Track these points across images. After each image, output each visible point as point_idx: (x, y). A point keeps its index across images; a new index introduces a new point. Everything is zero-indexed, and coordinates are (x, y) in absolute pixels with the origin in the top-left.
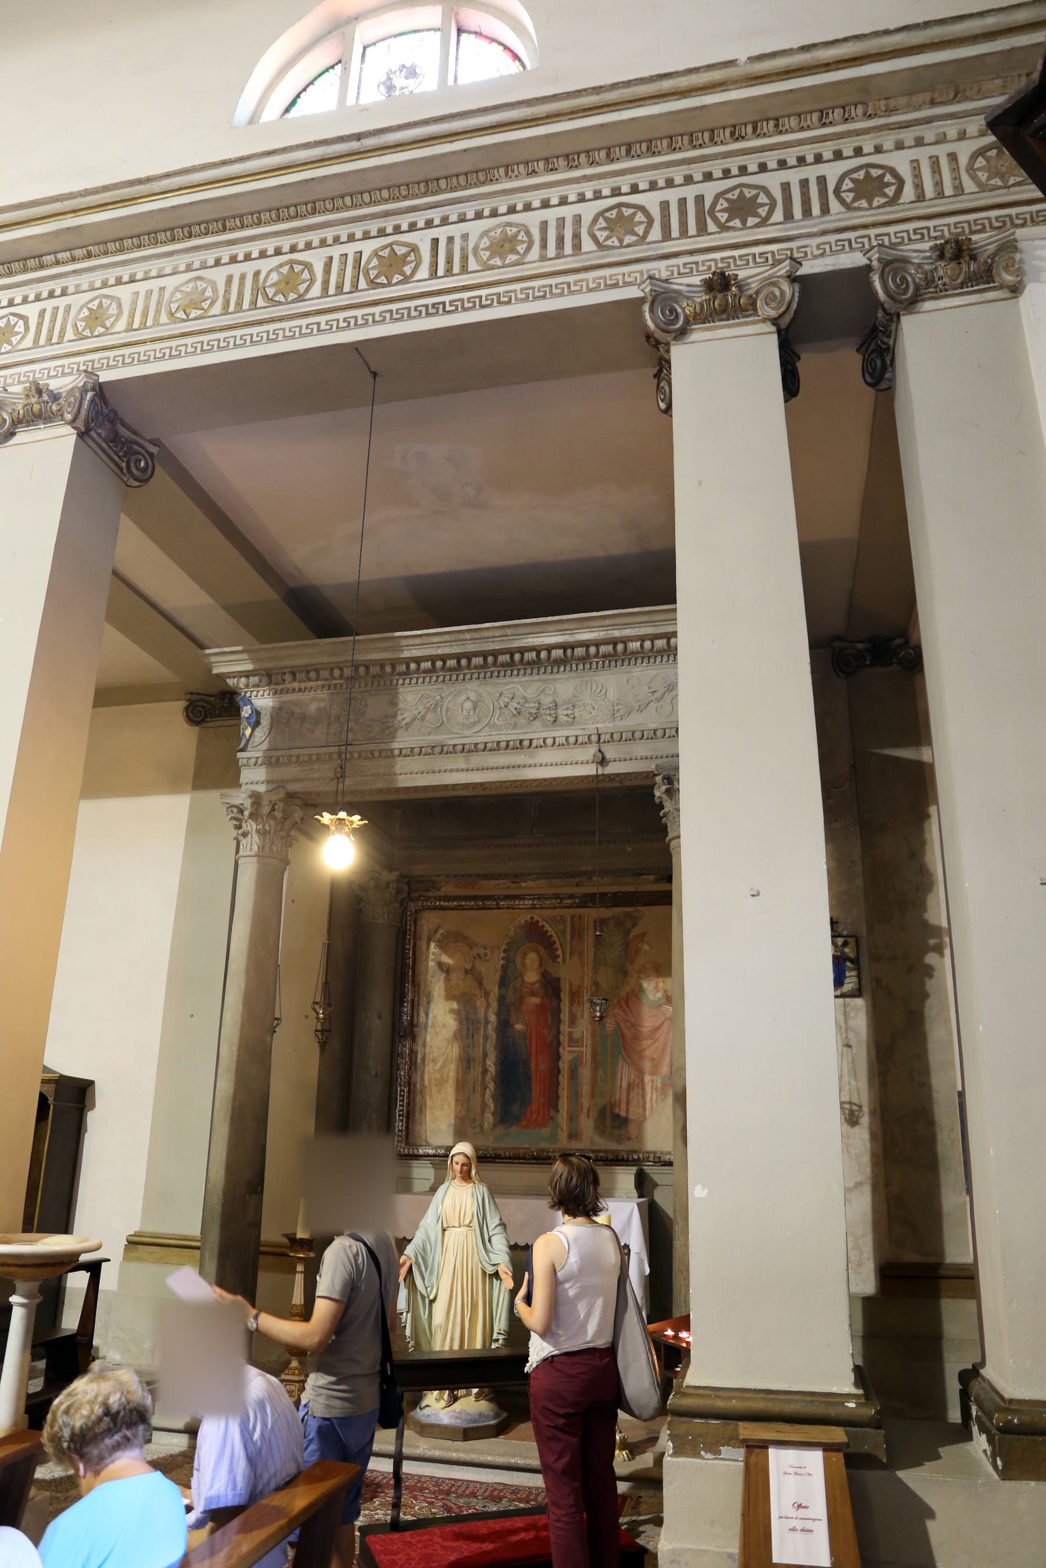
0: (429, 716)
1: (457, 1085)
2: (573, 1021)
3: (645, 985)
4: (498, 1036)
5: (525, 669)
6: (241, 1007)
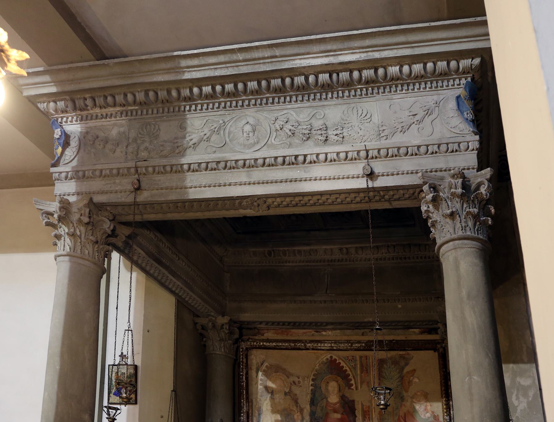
0: (214, 138)
3: (417, 407)
5: (297, 96)
6: (56, 386)
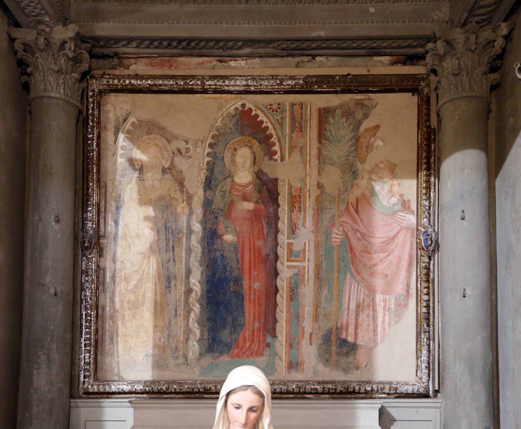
2: (293, 230)
4: (203, 248)
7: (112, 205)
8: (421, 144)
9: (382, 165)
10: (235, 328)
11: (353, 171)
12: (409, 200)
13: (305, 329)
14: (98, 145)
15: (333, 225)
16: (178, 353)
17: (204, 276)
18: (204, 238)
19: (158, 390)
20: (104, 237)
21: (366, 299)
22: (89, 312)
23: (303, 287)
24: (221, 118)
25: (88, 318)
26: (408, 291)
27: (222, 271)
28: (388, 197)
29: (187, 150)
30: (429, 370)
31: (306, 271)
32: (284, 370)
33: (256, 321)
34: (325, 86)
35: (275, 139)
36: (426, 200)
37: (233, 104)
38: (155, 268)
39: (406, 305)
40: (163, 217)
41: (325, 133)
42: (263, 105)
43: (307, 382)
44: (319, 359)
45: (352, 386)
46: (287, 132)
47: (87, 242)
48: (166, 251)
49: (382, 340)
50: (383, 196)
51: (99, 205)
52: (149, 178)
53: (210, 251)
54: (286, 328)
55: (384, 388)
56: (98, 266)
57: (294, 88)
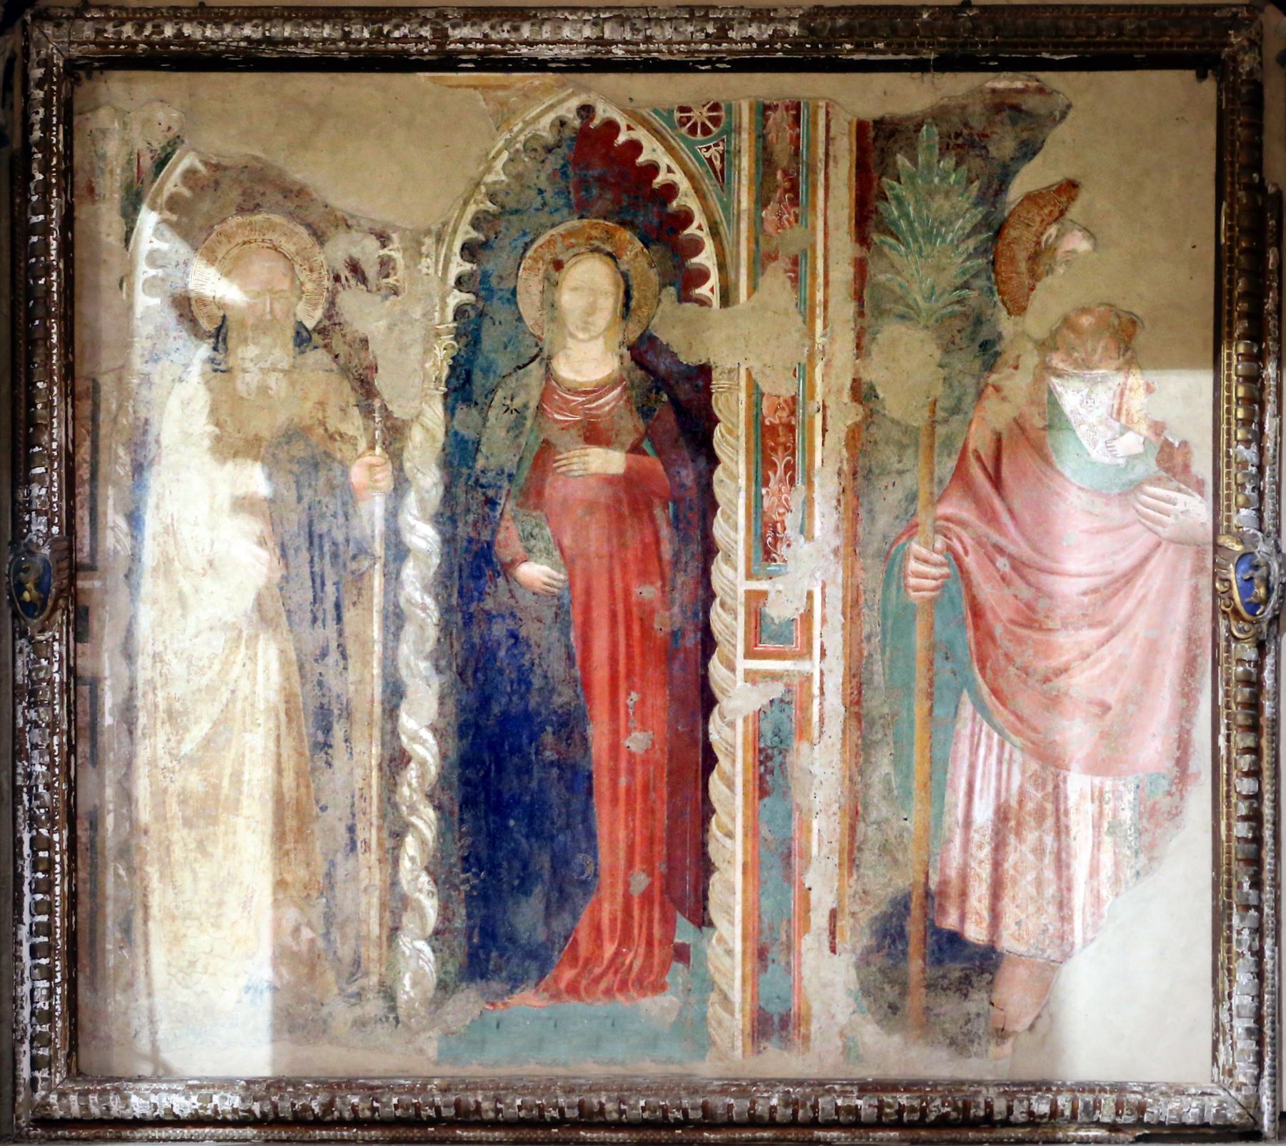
1: (279, 820)
2: (767, 545)
4: (446, 610)
7: (117, 457)
8: (1231, 249)
9: (1086, 321)
10: (561, 891)
11: (980, 340)
12: (1184, 444)
13: (814, 896)
14: (67, 249)
15: (911, 530)
16: (364, 982)
17: (450, 703)
18: (448, 575)
19: (295, 1113)
20: (92, 568)
21: (1030, 789)
22: (44, 831)
23: (804, 747)
24: (505, 156)
25: (41, 854)
26: (1182, 762)
27: (513, 692)
28: (1110, 435)
29: (386, 265)
30: (1260, 1043)
31: (816, 691)
32: (739, 1044)
33: (638, 866)
34: (881, 45)
35: (700, 228)
36: (1247, 443)
37: (550, 106)
38: (276, 679)
39: (1175, 814)
40: (300, 499)
41: (882, 206)
42: (656, 111)
43: (821, 1083)
44: (865, 1003)
45: (981, 1100)
46: (745, 204)
47: (29, 585)
48: (315, 620)
49: (1090, 935)
50: (1092, 426)
51: (70, 457)
52: (248, 365)
53: (469, 620)
54: (744, 891)
55: (1097, 1106)
56: (72, 671)
57: (767, 52)
